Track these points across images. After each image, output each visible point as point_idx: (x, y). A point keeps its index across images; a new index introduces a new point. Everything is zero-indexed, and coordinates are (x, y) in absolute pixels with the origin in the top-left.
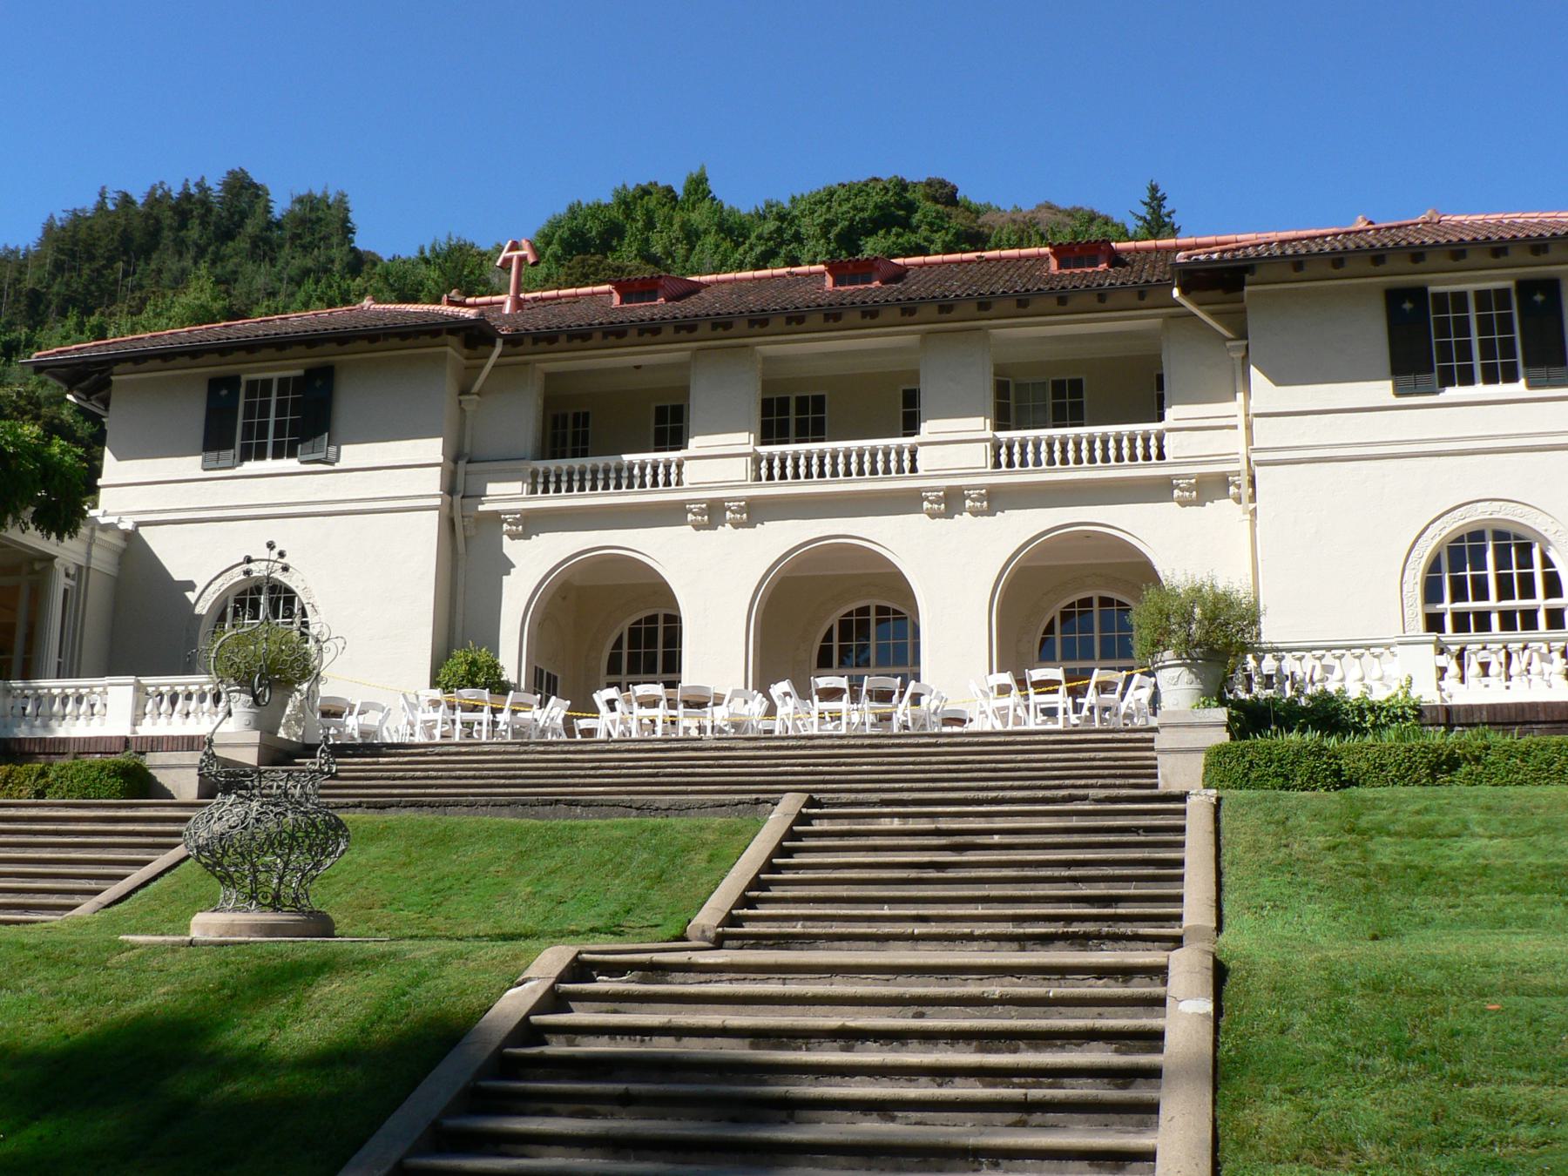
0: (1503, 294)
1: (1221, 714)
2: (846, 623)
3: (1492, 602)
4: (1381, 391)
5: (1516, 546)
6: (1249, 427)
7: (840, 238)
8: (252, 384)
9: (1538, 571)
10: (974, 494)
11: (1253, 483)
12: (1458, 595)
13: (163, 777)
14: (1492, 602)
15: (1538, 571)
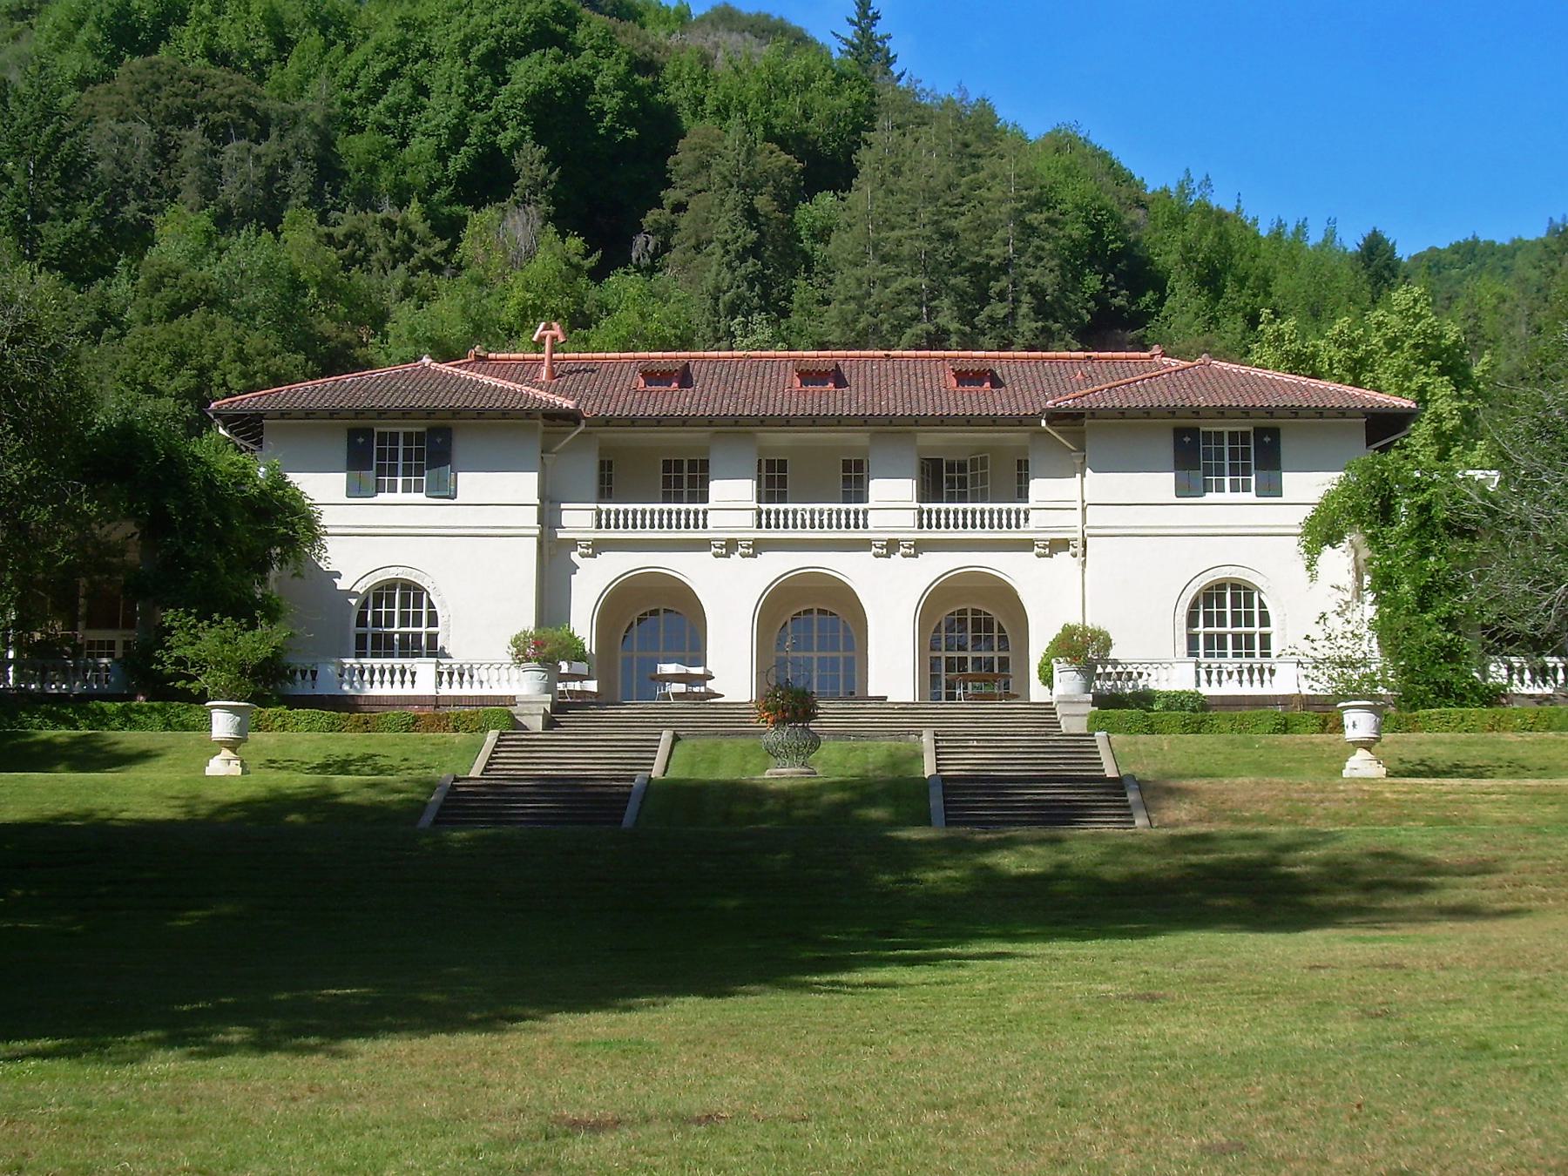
0: (1245, 434)
1: (1090, 697)
2: (812, 623)
3: (1228, 628)
4: (1163, 483)
5: (1243, 592)
6: (1084, 510)
7: (482, 61)
8: (382, 435)
9: (1256, 610)
10: (906, 544)
11: (1085, 545)
12: (1208, 623)
13: (523, 720)
14: (1228, 628)
15: (1256, 610)
